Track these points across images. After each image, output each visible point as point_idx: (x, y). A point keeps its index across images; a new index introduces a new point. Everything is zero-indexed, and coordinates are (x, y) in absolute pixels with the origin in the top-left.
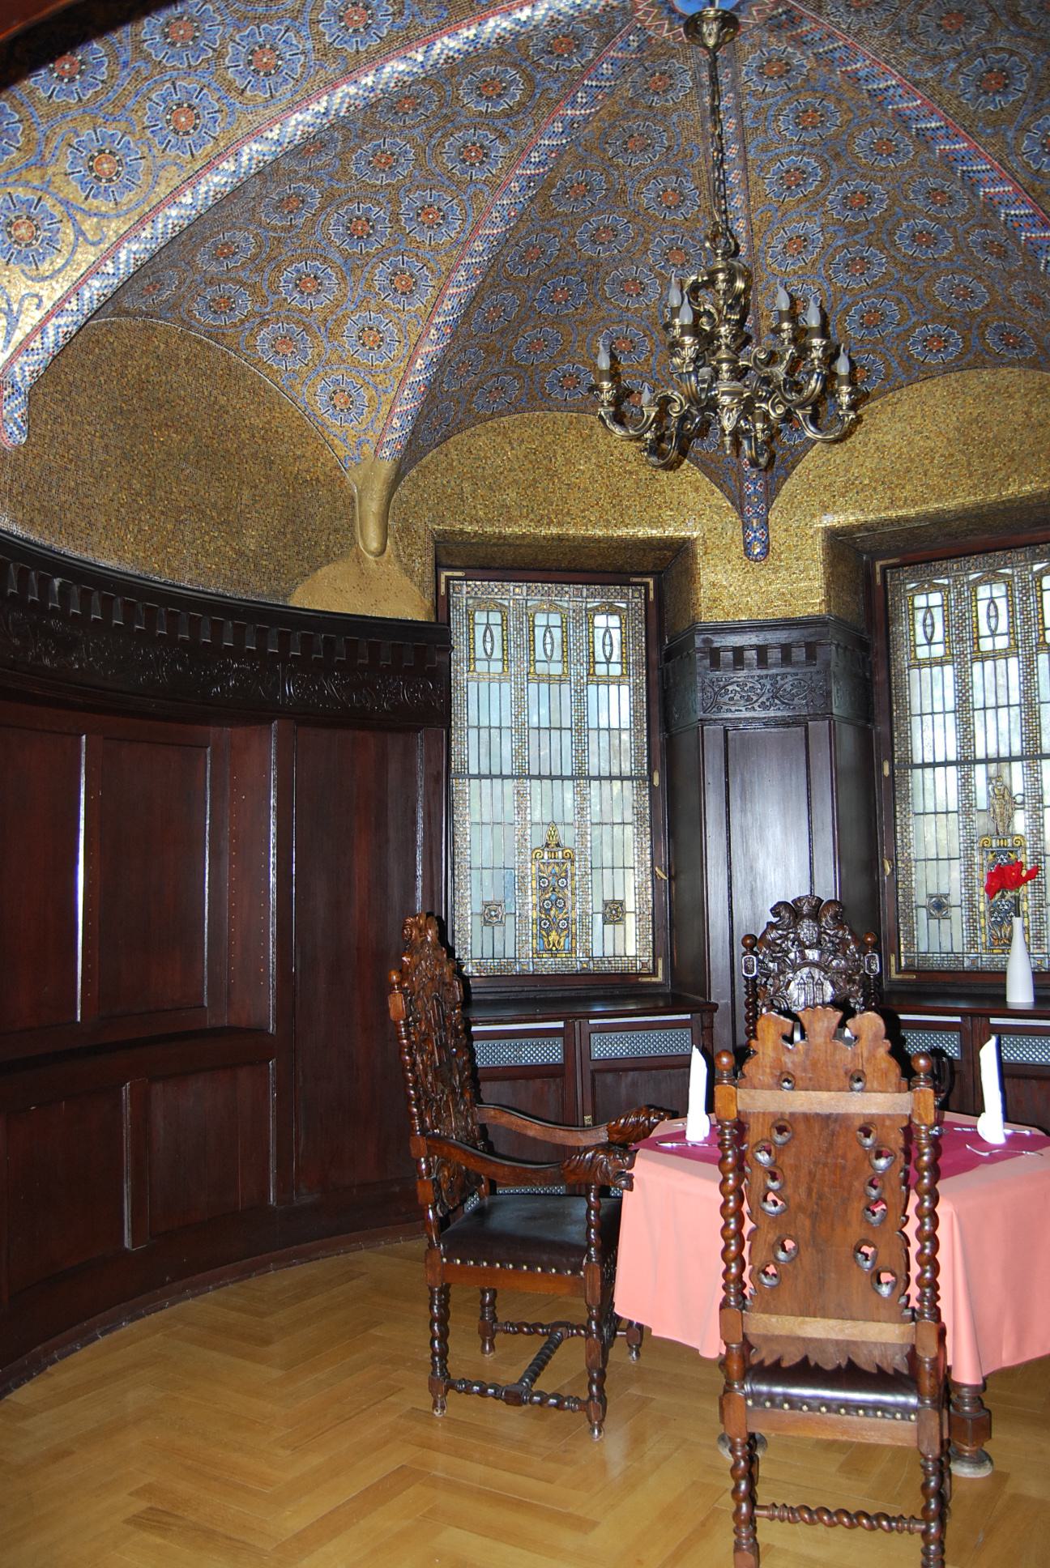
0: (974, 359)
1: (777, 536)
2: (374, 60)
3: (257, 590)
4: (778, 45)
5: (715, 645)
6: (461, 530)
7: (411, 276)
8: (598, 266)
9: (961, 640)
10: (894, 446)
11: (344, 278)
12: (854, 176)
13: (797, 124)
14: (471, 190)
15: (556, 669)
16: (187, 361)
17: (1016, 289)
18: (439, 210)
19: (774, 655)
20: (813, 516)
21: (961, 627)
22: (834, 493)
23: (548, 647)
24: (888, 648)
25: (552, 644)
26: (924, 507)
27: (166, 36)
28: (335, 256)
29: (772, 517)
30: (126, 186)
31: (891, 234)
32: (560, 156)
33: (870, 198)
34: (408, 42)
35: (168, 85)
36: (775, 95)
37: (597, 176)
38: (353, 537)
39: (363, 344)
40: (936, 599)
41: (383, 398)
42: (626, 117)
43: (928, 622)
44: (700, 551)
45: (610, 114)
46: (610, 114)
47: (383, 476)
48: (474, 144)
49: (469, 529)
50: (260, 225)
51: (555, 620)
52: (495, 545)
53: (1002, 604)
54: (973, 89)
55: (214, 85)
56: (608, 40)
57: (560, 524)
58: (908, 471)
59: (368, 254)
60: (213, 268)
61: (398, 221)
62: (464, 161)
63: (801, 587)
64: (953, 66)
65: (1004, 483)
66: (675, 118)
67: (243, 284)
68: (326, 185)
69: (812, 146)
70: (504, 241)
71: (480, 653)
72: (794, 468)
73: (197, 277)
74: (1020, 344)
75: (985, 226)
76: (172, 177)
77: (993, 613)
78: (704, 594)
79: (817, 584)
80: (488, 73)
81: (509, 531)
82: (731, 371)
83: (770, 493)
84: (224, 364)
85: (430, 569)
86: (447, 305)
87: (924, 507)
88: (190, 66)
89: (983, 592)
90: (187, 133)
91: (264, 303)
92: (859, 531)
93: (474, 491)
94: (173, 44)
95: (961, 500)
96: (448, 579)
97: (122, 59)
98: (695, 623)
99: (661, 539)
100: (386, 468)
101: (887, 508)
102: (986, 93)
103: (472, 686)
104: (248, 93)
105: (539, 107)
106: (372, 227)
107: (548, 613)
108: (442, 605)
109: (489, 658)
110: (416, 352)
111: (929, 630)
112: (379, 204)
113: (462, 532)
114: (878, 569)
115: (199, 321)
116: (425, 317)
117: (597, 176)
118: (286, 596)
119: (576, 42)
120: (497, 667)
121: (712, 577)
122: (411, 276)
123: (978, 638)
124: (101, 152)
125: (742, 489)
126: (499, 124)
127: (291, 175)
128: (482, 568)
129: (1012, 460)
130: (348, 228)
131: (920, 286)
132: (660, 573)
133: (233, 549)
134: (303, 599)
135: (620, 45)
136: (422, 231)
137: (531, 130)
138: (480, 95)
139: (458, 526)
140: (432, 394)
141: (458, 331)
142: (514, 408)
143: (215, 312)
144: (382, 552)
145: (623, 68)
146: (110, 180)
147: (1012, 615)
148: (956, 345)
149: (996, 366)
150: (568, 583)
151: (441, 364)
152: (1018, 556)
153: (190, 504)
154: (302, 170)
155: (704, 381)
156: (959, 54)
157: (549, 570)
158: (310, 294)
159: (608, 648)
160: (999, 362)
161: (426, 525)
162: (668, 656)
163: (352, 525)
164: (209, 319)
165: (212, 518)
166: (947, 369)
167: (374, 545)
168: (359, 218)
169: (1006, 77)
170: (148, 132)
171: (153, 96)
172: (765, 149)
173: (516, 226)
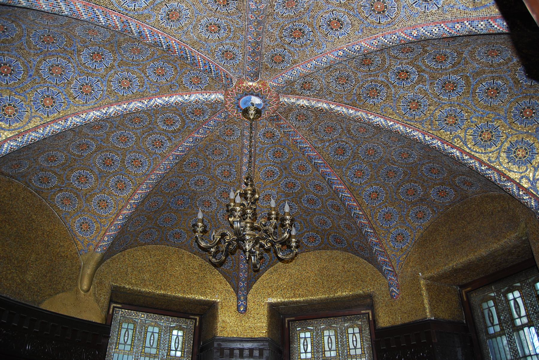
0: (324, 246)
1: (250, 305)
2: (129, 100)
3: (27, 298)
4: (271, 127)
5: (222, 347)
6: (124, 287)
7: (125, 184)
8: (196, 194)
9: (318, 352)
10: (295, 274)
11: (97, 180)
12: (290, 176)
13: (274, 155)
14: (154, 156)
15: (154, 351)
16: (23, 198)
17: (342, 222)
18: (141, 161)
19: (246, 353)
20: (264, 298)
21: (318, 347)
22: (272, 290)
23: (152, 341)
24: (290, 354)
25: (154, 340)
26: (306, 298)
27: (50, 70)
28: (97, 172)
29: (249, 296)
30: (16, 120)
31: (300, 198)
32: (190, 150)
33: (294, 185)
34: (143, 97)
35: (45, 88)
36: (268, 144)
37: (201, 161)
38: (77, 283)
39: (99, 206)
40: (308, 334)
41: (103, 228)
42: (215, 142)
43: (305, 344)
44: (219, 307)
45: (210, 139)
46: (210, 139)
47: (95, 259)
48: (159, 140)
49: (127, 287)
50: (69, 152)
51: (156, 330)
52: (137, 295)
53: (333, 338)
54: (333, 152)
55: (64, 93)
56: (214, 114)
57: (165, 290)
58: (300, 284)
59: (109, 172)
60: (45, 164)
61: (124, 162)
62: (154, 145)
63: (257, 325)
64: (328, 144)
65: (335, 291)
66: (232, 146)
67: (56, 173)
68: (99, 143)
69: (278, 164)
70: (163, 177)
71: (122, 341)
72: (258, 279)
73: (37, 166)
74: (341, 242)
75: (333, 199)
76: (36, 122)
77: (330, 342)
78: (219, 325)
79: (264, 325)
80: (169, 116)
81: (144, 290)
82: (250, 227)
83: (249, 287)
84: (39, 203)
85: (107, 302)
86: (136, 197)
87: (306, 298)
88: (56, 84)
89: (326, 333)
90: (48, 107)
91: (63, 183)
92: (281, 305)
93: (132, 272)
94: (52, 74)
95: (320, 296)
96: (114, 307)
97: (29, 74)
98: (215, 336)
99: (204, 300)
100: (98, 256)
101: (292, 297)
102: (337, 154)
103: (116, 355)
104: (77, 99)
105: (185, 132)
106: (113, 163)
107: (153, 328)
108: (109, 318)
109: (125, 343)
110: (120, 212)
111: (306, 347)
112: (118, 155)
113: (124, 287)
114: (286, 321)
115: (33, 184)
116: (126, 200)
117: (201, 161)
118: (39, 303)
119: (203, 112)
120: (128, 348)
121: (224, 318)
122: (125, 184)
123: (325, 351)
124: (9, 105)
125: (238, 284)
126: (169, 135)
127: (86, 135)
128: (129, 304)
129: (338, 283)
130: (104, 161)
131: (308, 218)
132: (202, 315)
133: (20, 278)
134: (46, 306)
135: (218, 115)
136: (132, 168)
137: (181, 139)
138: (165, 123)
139: (123, 285)
140: (123, 230)
141: (138, 207)
142: (154, 242)
143: (41, 182)
144: (88, 290)
145: (218, 124)
146: (10, 116)
147: (337, 343)
148: (319, 240)
149: (332, 249)
150: (164, 315)
151: (129, 218)
152: (339, 320)
153: (6, 256)
154: (91, 135)
155: (242, 227)
156: (330, 141)
157: (157, 309)
158: (82, 183)
159: (177, 344)
160: (333, 248)
161: (109, 282)
162: (202, 350)
163: (77, 277)
164: (38, 185)
165: (14, 264)
166: (315, 249)
167: (85, 287)
168: (109, 158)
169: (344, 150)
170: (32, 103)
171: (38, 90)
172: (262, 162)
173: (168, 172)
